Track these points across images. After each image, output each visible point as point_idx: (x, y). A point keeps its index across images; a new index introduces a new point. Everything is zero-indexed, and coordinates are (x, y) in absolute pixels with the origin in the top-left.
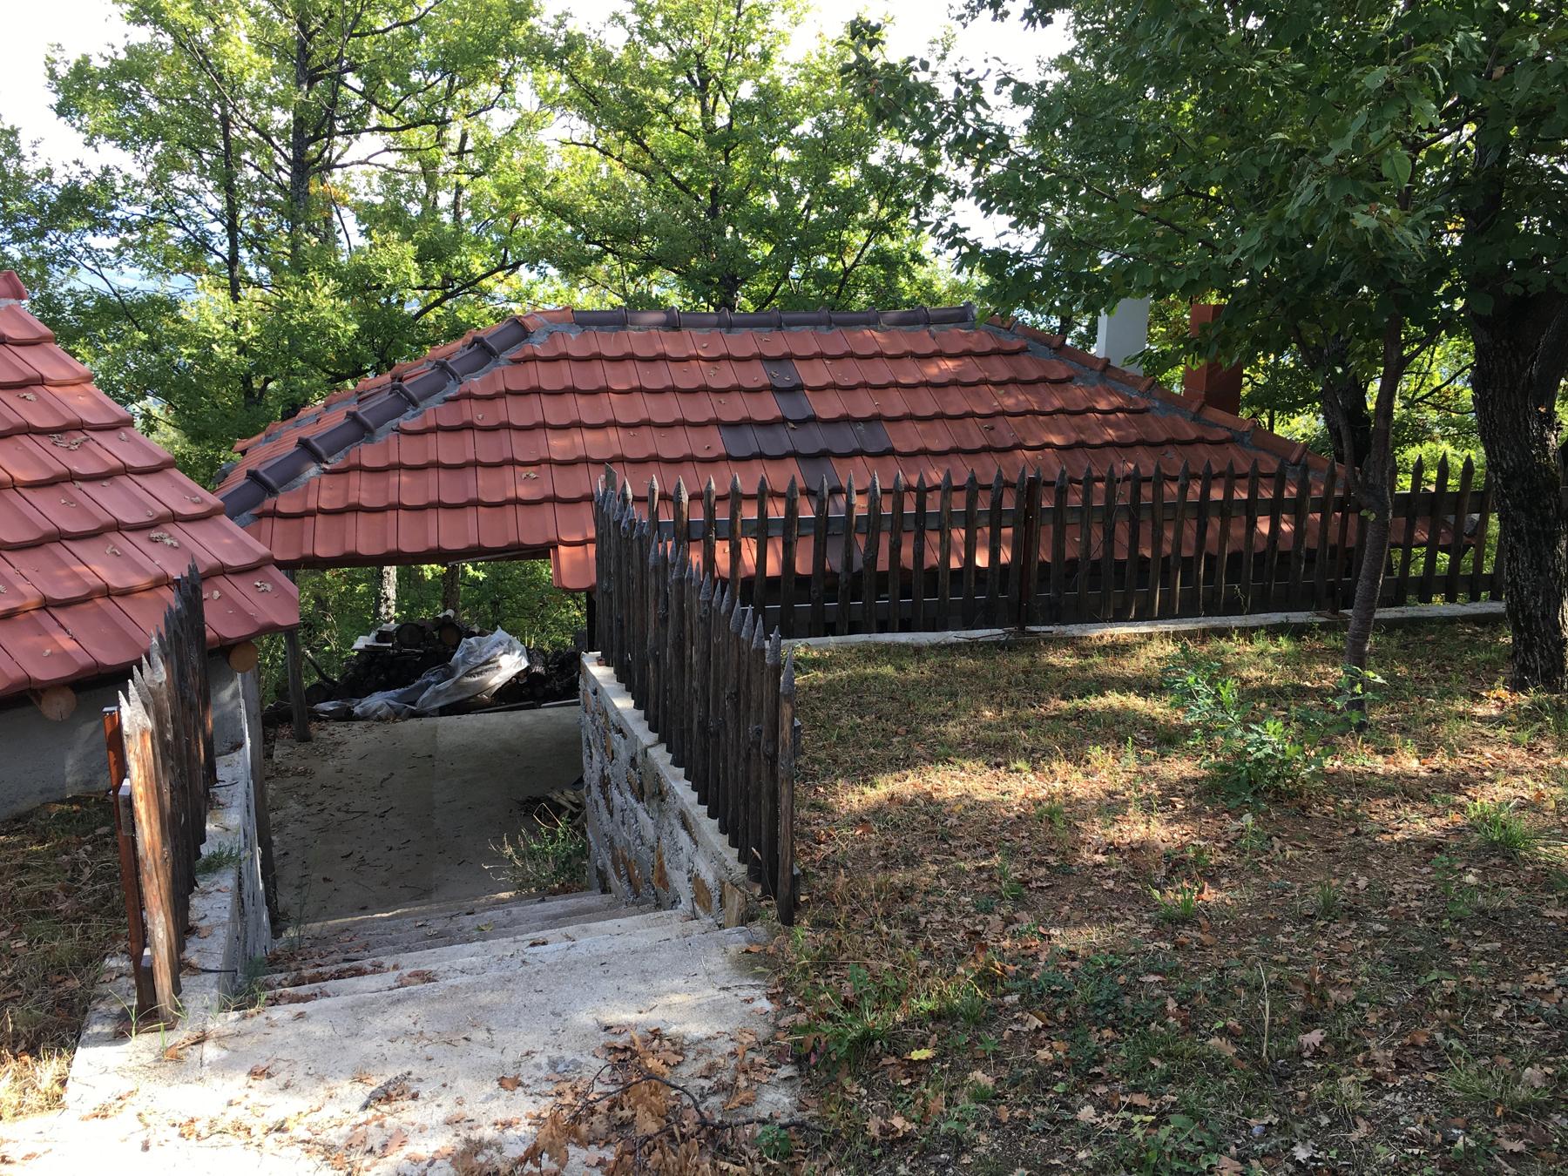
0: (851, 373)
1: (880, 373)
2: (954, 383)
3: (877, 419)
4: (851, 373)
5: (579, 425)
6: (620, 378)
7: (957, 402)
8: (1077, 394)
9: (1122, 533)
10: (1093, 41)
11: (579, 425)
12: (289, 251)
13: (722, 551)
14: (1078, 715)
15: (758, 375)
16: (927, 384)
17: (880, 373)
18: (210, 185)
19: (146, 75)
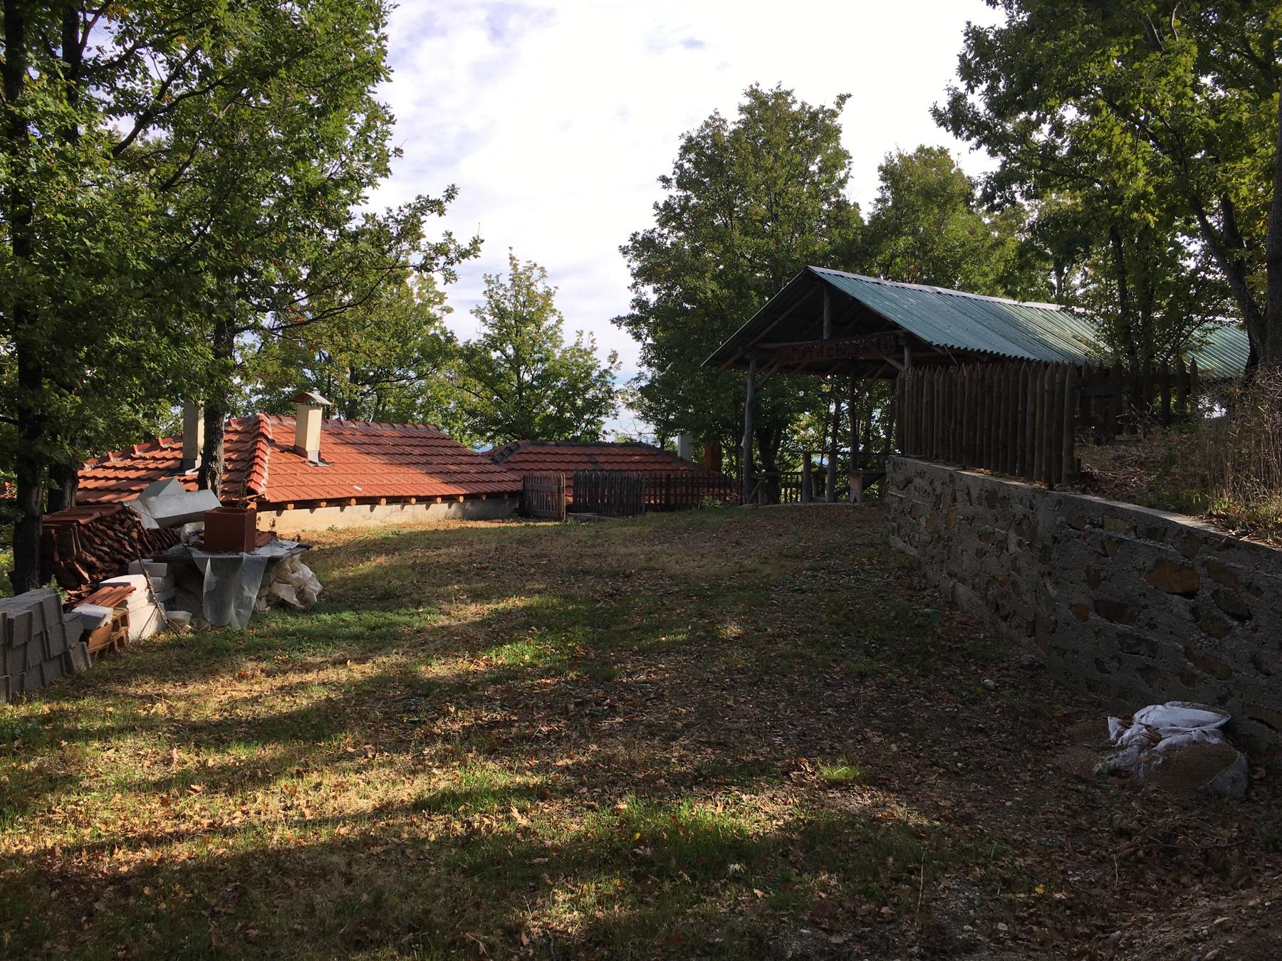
0: (611, 459)
1: (619, 459)
2: (639, 462)
3: (620, 470)
4: (611, 459)
5: (541, 469)
6: (549, 458)
7: (641, 467)
8: (674, 466)
9: (690, 498)
10: (108, 338)
11: (541, 469)
12: (15, 476)
13: (684, 491)
14: (1113, 508)
15: (585, 459)
16: (633, 462)
17: (619, 459)
18: (650, 340)
19: (722, 204)
